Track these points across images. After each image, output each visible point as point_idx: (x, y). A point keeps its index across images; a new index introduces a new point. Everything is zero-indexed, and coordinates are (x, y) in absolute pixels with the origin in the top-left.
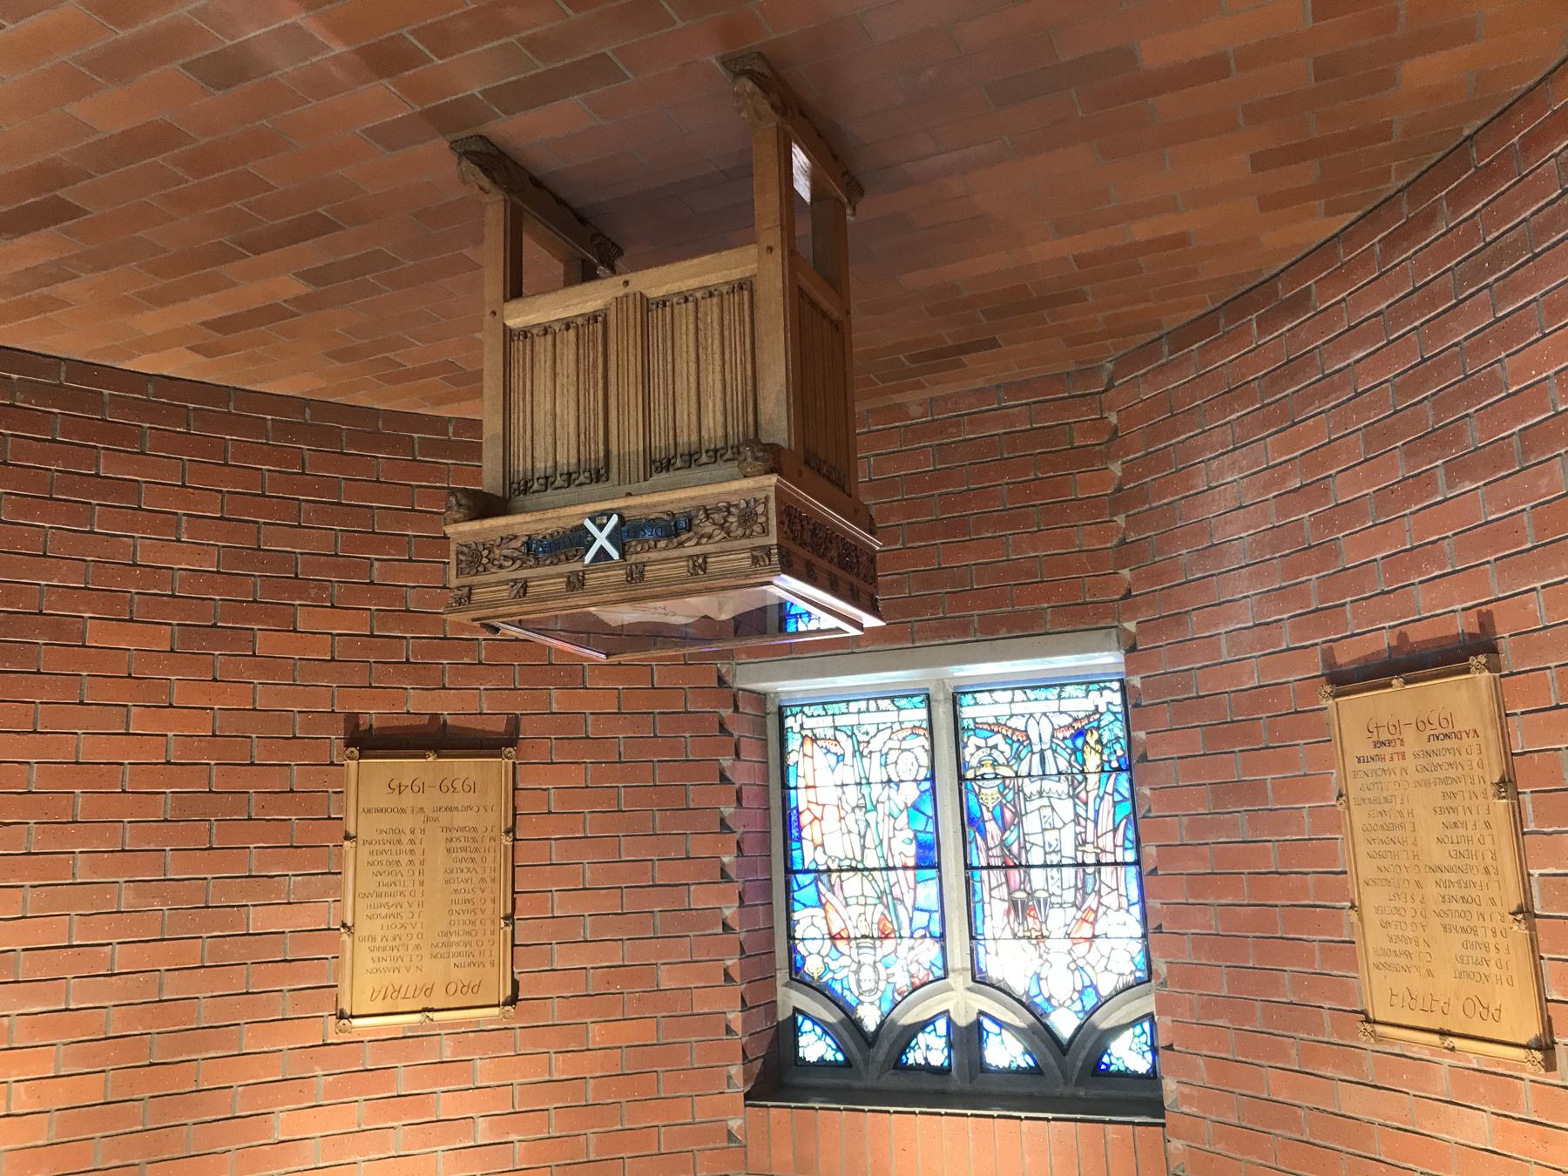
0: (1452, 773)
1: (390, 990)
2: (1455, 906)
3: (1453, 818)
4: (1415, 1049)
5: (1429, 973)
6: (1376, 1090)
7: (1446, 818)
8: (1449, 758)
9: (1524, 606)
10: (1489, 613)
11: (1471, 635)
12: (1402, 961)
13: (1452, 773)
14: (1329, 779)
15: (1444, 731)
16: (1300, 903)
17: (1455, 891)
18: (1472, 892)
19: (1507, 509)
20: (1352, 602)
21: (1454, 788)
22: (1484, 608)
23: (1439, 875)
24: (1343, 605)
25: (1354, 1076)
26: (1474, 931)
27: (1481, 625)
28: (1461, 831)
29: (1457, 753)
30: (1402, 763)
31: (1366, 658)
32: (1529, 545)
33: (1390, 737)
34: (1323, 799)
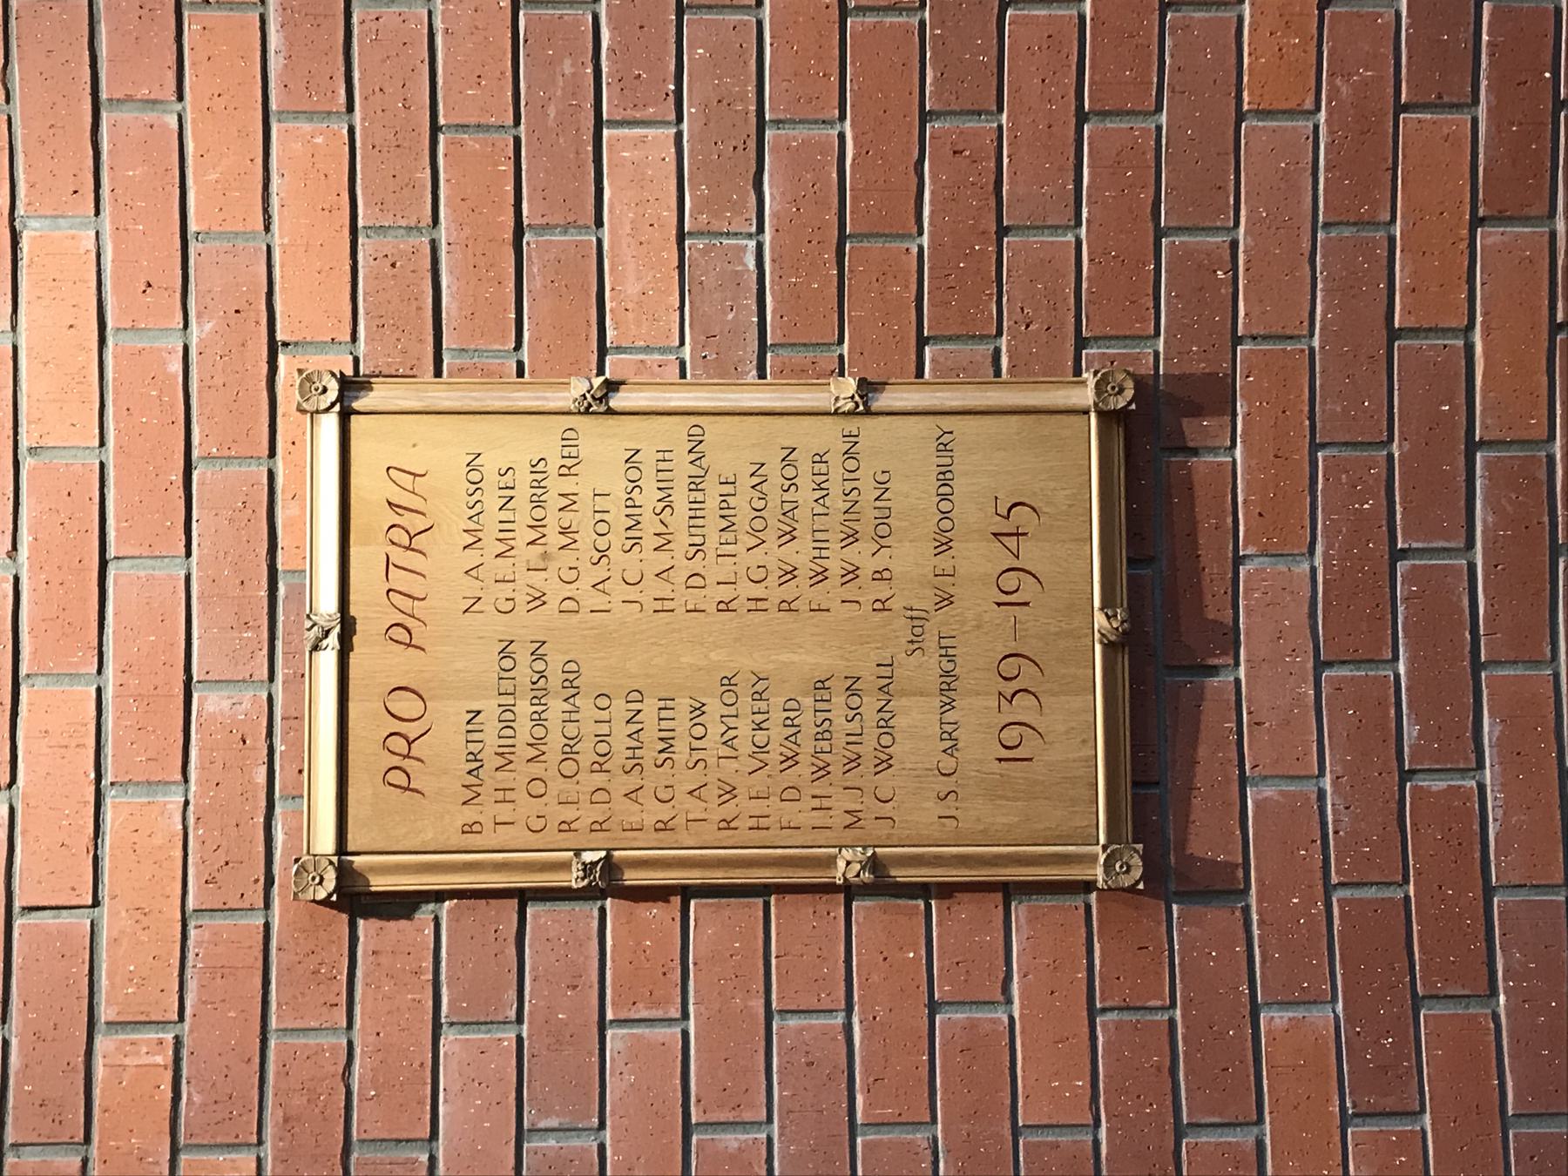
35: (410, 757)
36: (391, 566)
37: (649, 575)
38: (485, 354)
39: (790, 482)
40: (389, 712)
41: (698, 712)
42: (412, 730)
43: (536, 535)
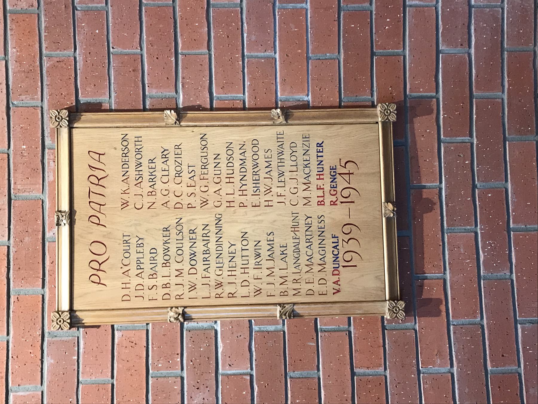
0: (303, 259)
1: (100, 174)
2: (187, 245)
3: (265, 253)
4: (52, 163)
5: (125, 204)
6: (4, 109)
7: (264, 247)
8: (317, 258)
9: (440, 354)
10: (438, 314)
11: (422, 286)
12: (132, 173)
13: (303, 259)
14: (303, 91)
15: (340, 255)
16: (179, 34)
17: (200, 247)
18: (200, 266)
19: (524, 348)
20: (472, 144)
21: (290, 259)
22: (443, 308)
23: (213, 229)
24: (471, 136)
25: (13, 83)
26: (166, 264)
27: (429, 301)
28: (252, 261)
29: (320, 268)
30: (314, 200)
31: (416, 158)
32: (489, 368)
33: (339, 189)
34: (284, 81)
35: (100, 270)
36: (91, 192)
37: (185, 194)
38: (343, 135)
39: (205, 146)
40: (92, 253)
41: (167, 251)
42: (101, 259)
43: (306, 187)
